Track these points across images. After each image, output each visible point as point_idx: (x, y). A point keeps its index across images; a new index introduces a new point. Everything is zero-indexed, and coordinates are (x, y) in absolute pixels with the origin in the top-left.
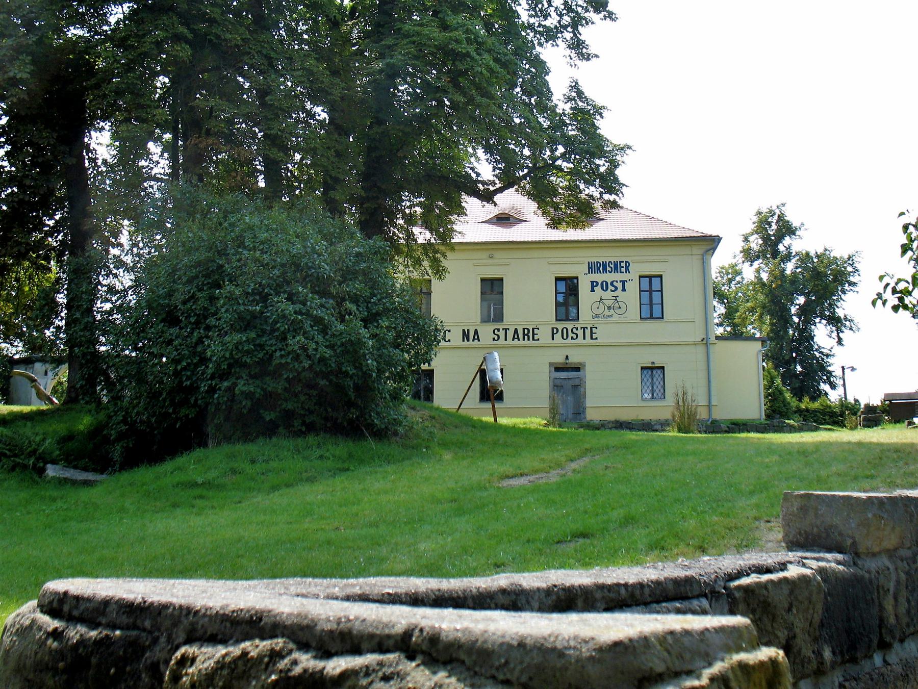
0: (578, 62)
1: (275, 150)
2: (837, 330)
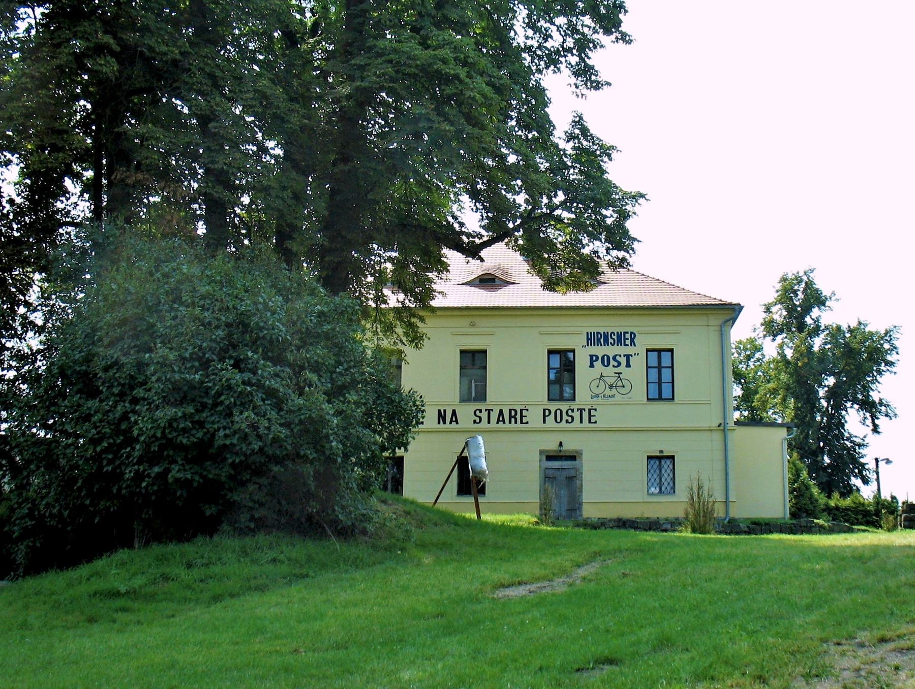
0: (585, 91)
1: (219, 188)
2: (871, 416)
